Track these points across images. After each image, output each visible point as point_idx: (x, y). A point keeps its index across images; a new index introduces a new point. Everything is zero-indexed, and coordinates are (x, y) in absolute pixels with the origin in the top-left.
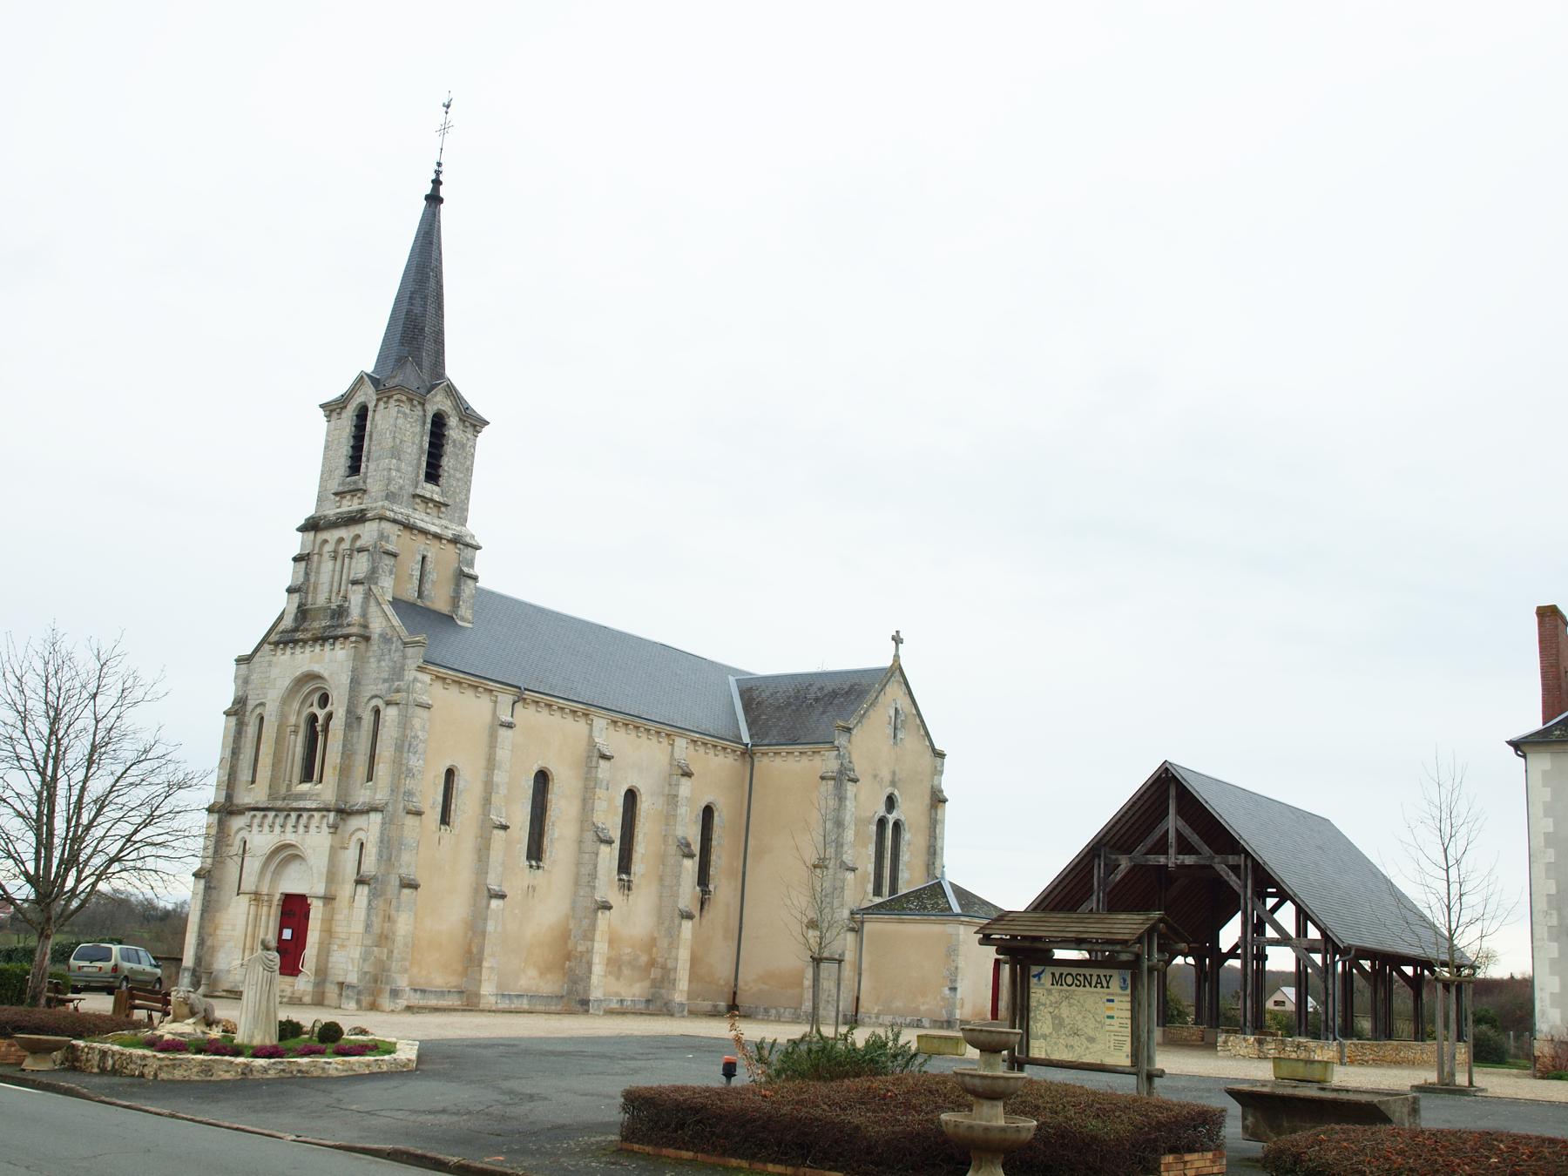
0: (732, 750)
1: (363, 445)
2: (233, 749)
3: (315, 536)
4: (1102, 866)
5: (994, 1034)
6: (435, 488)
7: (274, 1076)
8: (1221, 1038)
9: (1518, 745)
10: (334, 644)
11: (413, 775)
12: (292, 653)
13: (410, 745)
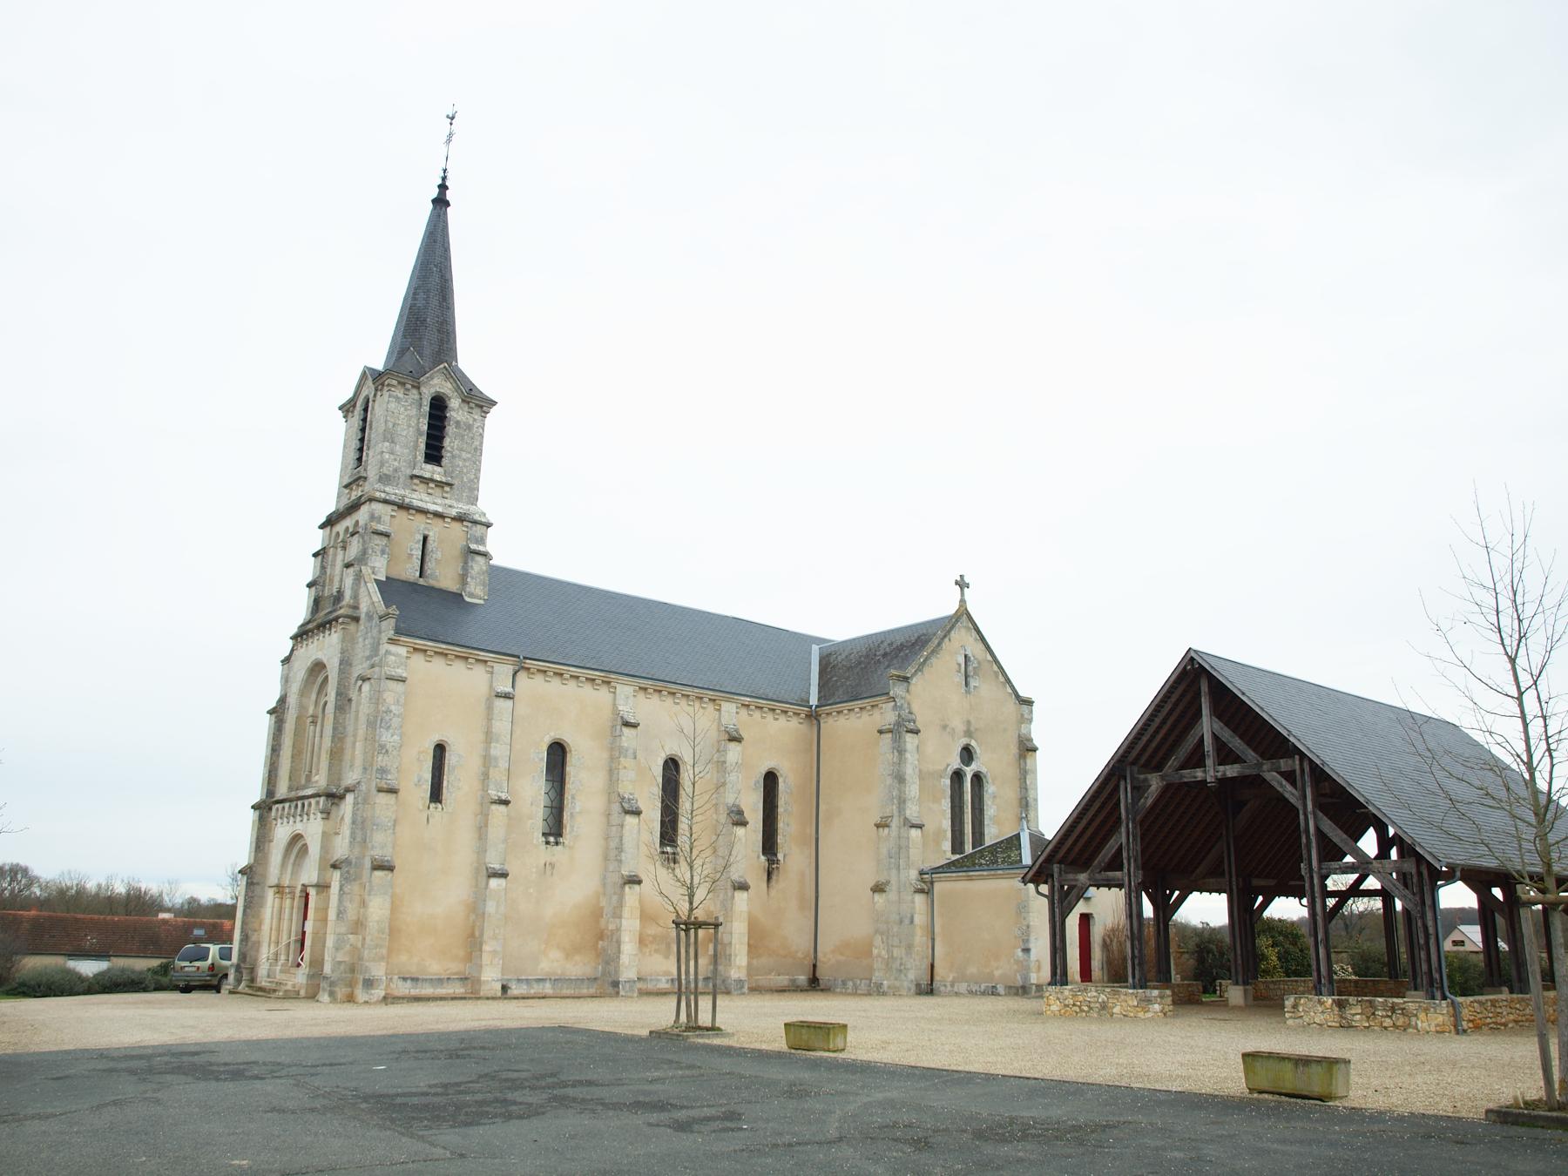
2: (273, 746)
3: (331, 530)
8: (1289, 1002)
11: (387, 751)
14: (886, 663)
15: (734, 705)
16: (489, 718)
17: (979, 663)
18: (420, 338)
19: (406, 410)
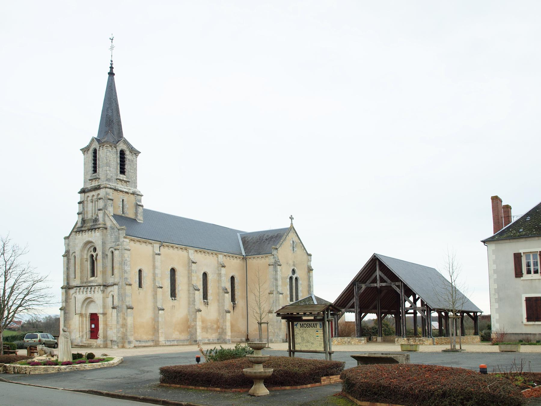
0: (239, 258)
1: (96, 163)
3: (84, 195)
5: (257, 344)
7: (68, 371)
8: (396, 339)
9: (484, 242)
10: (95, 231)
11: (127, 272)
12: (82, 235)
13: (124, 263)
14: (268, 243)
15: (222, 256)
17: (297, 243)
18: (112, 128)
19: (113, 155)
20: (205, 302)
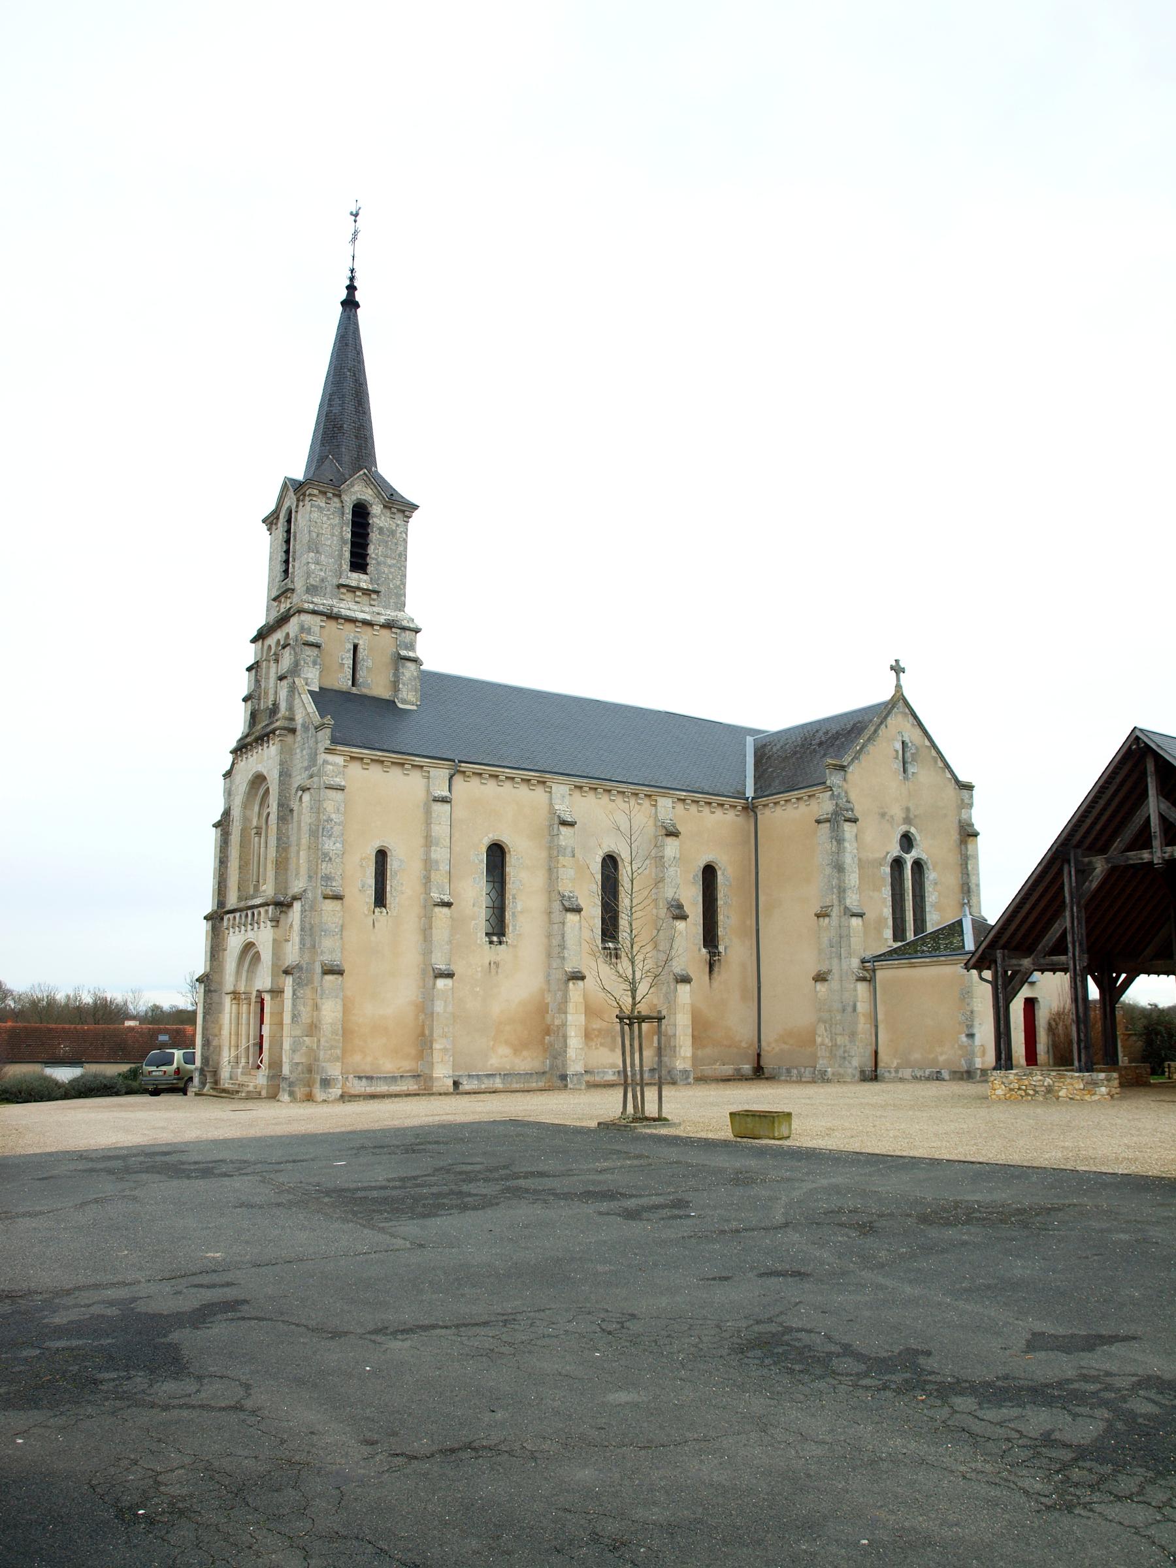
0: (718, 804)
3: (263, 644)
4: (1073, 873)
6: (362, 576)
11: (330, 859)
14: (822, 752)
15: (670, 800)
16: (428, 823)
17: (917, 748)
19: (328, 519)
20: (609, 948)
